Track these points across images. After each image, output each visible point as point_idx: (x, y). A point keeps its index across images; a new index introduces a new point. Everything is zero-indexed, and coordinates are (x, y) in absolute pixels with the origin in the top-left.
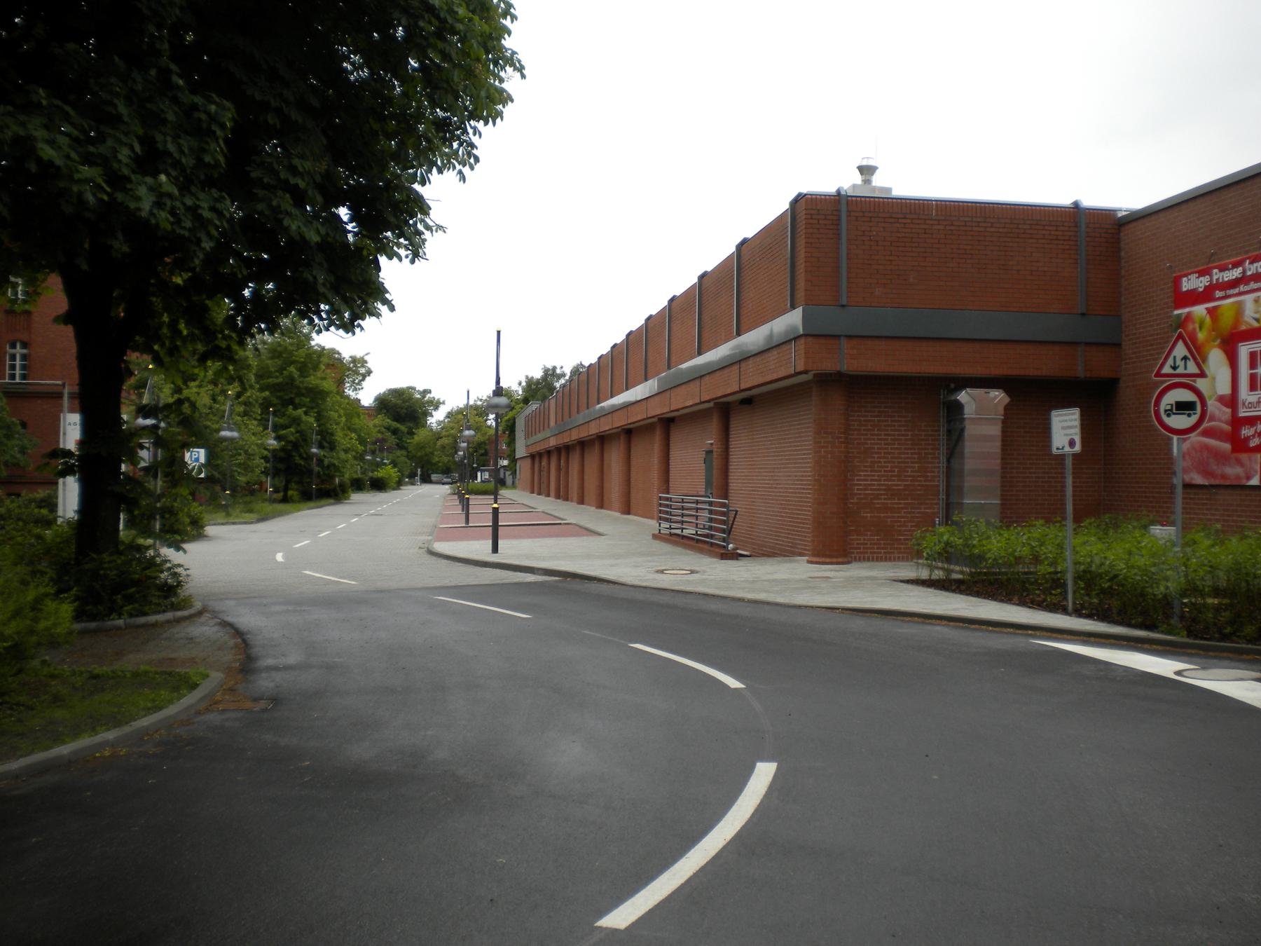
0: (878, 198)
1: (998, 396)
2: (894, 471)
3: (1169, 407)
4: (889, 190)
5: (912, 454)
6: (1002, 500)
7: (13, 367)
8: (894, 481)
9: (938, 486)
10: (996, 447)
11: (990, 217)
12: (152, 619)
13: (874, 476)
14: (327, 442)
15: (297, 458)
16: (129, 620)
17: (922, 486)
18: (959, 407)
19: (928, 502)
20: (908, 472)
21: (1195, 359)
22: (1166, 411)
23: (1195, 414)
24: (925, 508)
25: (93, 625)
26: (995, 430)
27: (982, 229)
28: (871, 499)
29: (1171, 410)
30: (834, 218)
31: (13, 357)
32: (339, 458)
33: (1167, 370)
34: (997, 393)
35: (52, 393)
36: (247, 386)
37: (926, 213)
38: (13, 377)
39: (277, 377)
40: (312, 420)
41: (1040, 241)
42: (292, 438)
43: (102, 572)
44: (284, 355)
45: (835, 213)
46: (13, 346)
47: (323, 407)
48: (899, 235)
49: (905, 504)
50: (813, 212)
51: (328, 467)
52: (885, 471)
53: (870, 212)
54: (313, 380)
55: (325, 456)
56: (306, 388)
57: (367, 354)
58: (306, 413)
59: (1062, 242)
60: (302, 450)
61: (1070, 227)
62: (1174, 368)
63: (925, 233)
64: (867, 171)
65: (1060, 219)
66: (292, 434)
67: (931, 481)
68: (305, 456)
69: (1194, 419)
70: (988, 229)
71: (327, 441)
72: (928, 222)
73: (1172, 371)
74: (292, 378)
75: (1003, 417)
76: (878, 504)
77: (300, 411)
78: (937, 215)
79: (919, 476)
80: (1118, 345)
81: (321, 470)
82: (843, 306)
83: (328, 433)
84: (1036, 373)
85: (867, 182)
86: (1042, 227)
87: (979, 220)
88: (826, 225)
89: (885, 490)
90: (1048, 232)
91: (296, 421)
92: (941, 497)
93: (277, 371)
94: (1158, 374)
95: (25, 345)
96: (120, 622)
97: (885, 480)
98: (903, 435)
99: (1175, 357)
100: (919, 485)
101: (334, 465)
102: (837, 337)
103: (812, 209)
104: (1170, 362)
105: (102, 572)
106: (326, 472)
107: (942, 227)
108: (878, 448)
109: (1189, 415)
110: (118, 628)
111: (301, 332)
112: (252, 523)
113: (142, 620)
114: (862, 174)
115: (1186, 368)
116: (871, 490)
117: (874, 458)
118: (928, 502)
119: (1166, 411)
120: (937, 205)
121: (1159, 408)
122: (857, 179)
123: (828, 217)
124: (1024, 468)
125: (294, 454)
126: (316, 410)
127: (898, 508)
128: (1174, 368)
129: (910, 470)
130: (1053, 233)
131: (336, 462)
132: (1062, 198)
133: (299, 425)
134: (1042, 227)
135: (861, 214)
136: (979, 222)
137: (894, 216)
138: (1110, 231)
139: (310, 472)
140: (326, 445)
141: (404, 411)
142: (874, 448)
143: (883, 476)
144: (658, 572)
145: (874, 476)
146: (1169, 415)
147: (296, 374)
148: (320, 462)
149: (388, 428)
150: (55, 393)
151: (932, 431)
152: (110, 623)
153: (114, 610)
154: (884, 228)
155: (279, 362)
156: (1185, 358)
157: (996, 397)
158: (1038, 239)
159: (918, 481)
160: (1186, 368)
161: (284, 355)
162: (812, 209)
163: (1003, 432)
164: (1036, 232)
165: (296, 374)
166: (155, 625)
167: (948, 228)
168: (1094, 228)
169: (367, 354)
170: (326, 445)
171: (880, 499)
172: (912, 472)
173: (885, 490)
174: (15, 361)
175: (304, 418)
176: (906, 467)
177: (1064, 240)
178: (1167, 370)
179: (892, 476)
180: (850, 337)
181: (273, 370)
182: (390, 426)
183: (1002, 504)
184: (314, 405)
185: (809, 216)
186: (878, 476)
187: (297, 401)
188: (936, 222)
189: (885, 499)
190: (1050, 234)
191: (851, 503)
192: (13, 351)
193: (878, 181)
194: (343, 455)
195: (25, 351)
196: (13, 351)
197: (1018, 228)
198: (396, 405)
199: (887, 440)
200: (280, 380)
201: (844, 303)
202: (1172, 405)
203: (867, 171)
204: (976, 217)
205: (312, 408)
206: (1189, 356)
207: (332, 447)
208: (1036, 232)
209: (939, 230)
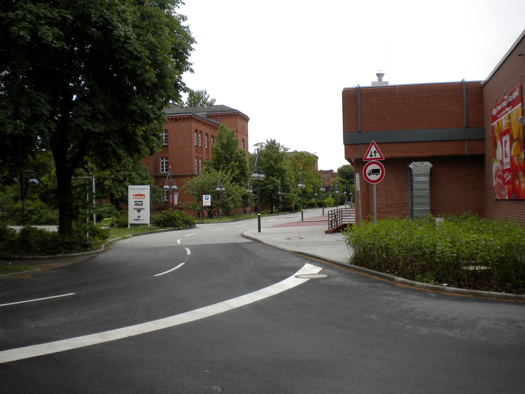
0: (383, 87)
1: (428, 165)
2: (389, 197)
3: (369, 172)
4: (387, 82)
5: (396, 190)
6: (430, 208)
7: (163, 167)
8: (389, 201)
9: (408, 202)
10: (427, 186)
11: (422, 90)
12: (73, 254)
13: (380, 199)
14: (286, 189)
15: (274, 196)
16: (63, 255)
17: (402, 202)
18: (411, 170)
19: (404, 209)
20: (395, 197)
21: (379, 152)
22: (368, 173)
23: (379, 174)
24: (403, 212)
25: (51, 256)
26: (427, 179)
27: (418, 96)
28: (379, 209)
29: (370, 173)
30: (355, 97)
31: (163, 163)
32: (291, 196)
33: (368, 157)
34: (427, 163)
35: (176, 176)
36: (245, 170)
37: (394, 91)
38: (163, 170)
39: (266, 165)
40: (279, 181)
41: (446, 98)
42: (271, 188)
43: (56, 240)
44: (269, 156)
45: (355, 95)
46: (163, 159)
47: (284, 176)
48: (382, 101)
49: (394, 210)
50: (346, 96)
51: (287, 199)
52: (385, 197)
53: (370, 93)
54: (279, 166)
55: (285, 195)
56: (277, 169)
57: (315, 153)
58: (277, 178)
59: (455, 98)
60: (276, 193)
61: (459, 91)
62: (371, 156)
63: (394, 100)
64: (380, 75)
65: (454, 88)
66: (271, 187)
67: (405, 201)
68: (277, 195)
69: (379, 176)
70: (421, 96)
71: (285, 188)
72: (395, 95)
73: (370, 158)
74: (271, 164)
75: (429, 173)
76: (383, 210)
77: (275, 178)
78: (399, 91)
79: (400, 199)
80: (484, 140)
81: (283, 200)
82: (360, 132)
83: (287, 186)
84: (445, 154)
85: (380, 80)
86: (446, 92)
87: (417, 92)
88: (352, 100)
89: (385, 205)
90: (449, 94)
91: (273, 182)
92: (409, 207)
93: (266, 163)
94: (365, 159)
95: (166, 159)
96: (61, 255)
97: (385, 201)
98: (393, 182)
99: (371, 152)
100: (400, 202)
101: (289, 198)
102: (358, 144)
103: (346, 95)
104: (370, 154)
105: (56, 240)
106: (286, 201)
107: (401, 97)
108: (382, 188)
109: (377, 175)
110: (60, 257)
111: (276, 147)
112: (228, 222)
113: (69, 255)
114: (378, 77)
115: (375, 156)
116: (380, 205)
117: (380, 192)
118: (404, 209)
119: (368, 173)
120: (398, 88)
121: (366, 172)
122: (376, 79)
123: (353, 97)
124: (444, 192)
125: (273, 195)
126: (281, 177)
127: (391, 212)
128: (371, 156)
129: (396, 196)
130: (451, 94)
131: (289, 197)
132: (458, 79)
133: (274, 183)
134: (446, 92)
135: (366, 95)
136: (417, 93)
137: (380, 94)
138: (478, 91)
139: (279, 201)
140: (286, 190)
141: (350, 174)
142: (380, 188)
143: (384, 199)
144: (287, 239)
145: (380, 199)
146: (369, 175)
147: (273, 163)
148: (283, 197)
149: (341, 182)
150: (178, 176)
151: (405, 180)
152: (57, 256)
153: (60, 252)
154: (376, 99)
155: (267, 159)
156: (375, 152)
157: (426, 165)
158: (444, 97)
159: (399, 201)
160: (375, 156)
161: (269, 156)
162: (346, 95)
163: (430, 179)
164: (443, 94)
165: (273, 163)
166: (73, 257)
167: (404, 96)
168: (470, 90)
169: (315, 153)
170: (286, 190)
171: (384, 208)
172: (397, 197)
173: (385, 205)
174: (163, 164)
175: (276, 180)
176: (394, 195)
177: (457, 97)
178: (368, 157)
179: (388, 199)
180: (363, 144)
181: (264, 162)
182: (341, 181)
183: (431, 209)
184: (281, 175)
185: (345, 98)
186: (382, 199)
187: (274, 174)
188: (398, 95)
189: (385, 208)
190: (450, 95)
191: (371, 210)
192: (162, 161)
193: (384, 79)
194: (293, 194)
195: (167, 161)
196: (162, 161)
197: (435, 94)
198: (346, 172)
199: (386, 184)
200: (268, 166)
201: (360, 131)
202: (370, 171)
203: (380, 75)
204: (416, 91)
205: (280, 176)
206: (376, 151)
207: (288, 191)
208: (443, 94)
209: (400, 98)
